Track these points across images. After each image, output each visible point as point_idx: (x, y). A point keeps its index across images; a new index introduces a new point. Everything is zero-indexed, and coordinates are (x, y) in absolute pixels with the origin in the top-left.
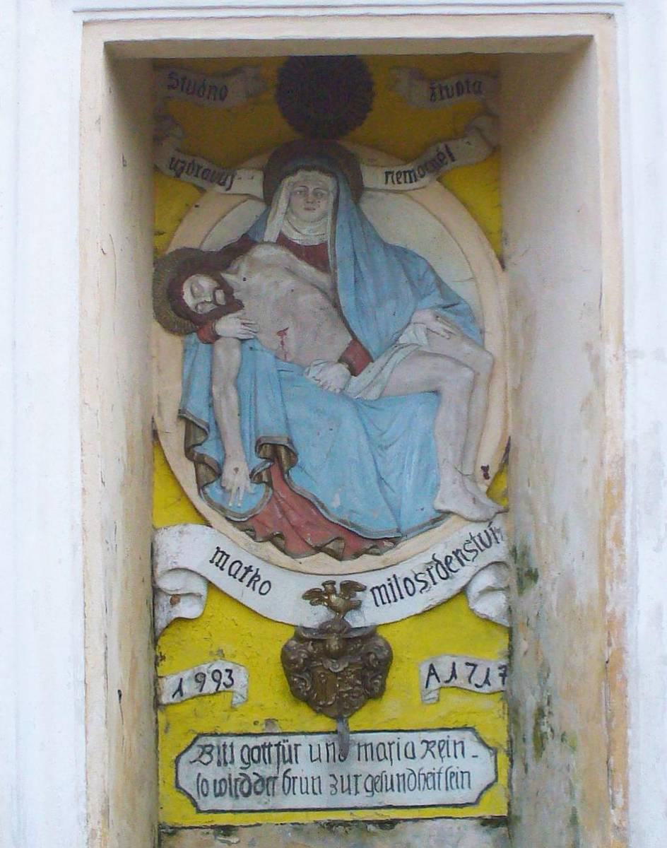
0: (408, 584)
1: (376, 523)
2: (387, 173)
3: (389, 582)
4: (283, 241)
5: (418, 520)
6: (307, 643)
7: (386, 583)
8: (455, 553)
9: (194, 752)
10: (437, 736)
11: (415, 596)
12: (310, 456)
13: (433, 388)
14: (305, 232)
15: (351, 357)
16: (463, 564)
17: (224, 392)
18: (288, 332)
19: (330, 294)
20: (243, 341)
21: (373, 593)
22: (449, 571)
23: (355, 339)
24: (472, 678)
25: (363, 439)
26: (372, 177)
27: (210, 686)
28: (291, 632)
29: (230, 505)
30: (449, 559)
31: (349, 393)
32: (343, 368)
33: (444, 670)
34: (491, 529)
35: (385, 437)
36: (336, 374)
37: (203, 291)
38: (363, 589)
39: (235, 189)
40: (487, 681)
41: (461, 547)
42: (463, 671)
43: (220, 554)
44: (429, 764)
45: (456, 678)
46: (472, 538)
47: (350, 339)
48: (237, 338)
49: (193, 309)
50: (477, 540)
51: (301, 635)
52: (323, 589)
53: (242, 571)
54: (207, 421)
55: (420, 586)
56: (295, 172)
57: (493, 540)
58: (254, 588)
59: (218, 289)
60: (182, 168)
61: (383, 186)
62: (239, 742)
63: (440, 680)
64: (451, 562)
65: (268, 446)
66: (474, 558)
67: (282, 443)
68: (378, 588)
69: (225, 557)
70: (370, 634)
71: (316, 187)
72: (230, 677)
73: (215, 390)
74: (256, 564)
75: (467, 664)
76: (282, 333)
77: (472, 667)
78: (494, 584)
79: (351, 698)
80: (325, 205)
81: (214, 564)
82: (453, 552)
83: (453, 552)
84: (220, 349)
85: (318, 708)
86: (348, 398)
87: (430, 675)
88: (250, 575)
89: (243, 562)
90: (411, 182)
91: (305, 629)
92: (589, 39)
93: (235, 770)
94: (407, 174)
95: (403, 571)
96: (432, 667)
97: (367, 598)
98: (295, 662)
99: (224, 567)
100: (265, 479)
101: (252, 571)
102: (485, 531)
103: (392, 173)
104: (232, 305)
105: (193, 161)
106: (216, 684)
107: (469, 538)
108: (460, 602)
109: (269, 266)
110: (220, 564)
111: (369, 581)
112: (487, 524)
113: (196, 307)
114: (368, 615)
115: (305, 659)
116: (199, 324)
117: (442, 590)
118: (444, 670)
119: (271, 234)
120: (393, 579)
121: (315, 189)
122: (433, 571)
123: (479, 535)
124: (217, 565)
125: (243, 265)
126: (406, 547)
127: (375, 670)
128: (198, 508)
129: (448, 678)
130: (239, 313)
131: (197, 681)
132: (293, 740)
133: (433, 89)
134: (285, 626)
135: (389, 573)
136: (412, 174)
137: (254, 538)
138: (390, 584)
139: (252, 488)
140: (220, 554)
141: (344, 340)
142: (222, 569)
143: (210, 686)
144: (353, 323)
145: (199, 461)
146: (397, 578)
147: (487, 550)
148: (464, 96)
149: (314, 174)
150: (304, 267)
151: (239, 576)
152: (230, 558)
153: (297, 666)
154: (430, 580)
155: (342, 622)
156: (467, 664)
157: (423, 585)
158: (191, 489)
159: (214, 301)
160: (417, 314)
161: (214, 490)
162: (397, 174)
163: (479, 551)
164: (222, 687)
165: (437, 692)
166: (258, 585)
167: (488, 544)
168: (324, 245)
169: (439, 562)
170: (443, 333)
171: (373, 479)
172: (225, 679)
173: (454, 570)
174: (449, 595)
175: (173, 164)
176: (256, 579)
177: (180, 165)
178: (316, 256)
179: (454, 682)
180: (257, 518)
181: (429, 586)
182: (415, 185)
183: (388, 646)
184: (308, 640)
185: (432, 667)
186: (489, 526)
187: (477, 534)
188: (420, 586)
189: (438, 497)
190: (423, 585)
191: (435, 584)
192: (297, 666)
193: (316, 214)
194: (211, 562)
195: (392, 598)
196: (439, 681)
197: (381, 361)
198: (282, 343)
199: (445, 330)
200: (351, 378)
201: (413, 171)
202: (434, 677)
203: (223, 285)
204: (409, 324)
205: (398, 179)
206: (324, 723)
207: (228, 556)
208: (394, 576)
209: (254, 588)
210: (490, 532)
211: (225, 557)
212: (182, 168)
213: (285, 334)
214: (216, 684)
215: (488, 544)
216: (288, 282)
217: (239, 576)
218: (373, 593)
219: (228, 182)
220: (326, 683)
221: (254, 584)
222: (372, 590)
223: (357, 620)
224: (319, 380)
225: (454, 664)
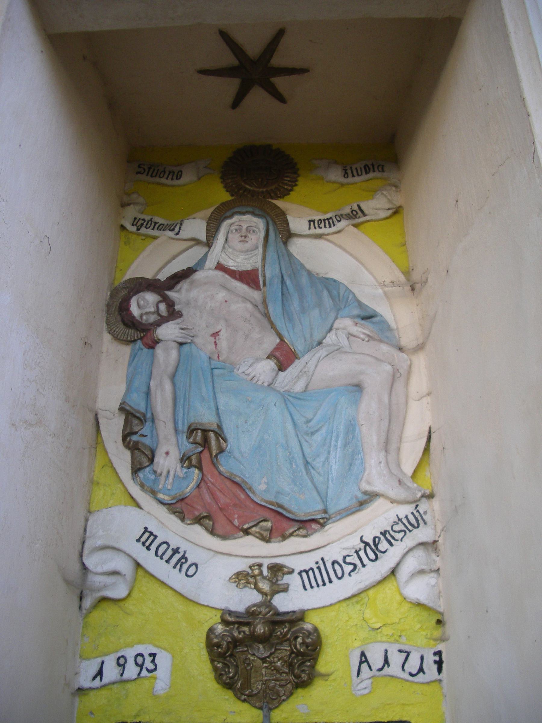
0: (337, 567)
2: (310, 221)
3: (317, 565)
4: (220, 267)
5: (344, 503)
6: (232, 627)
7: (315, 567)
8: (384, 533)
11: (343, 579)
13: (355, 381)
14: (239, 260)
15: (278, 354)
16: (391, 544)
17: (161, 384)
18: (221, 333)
19: (261, 307)
20: (181, 344)
21: (301, 577)
22: (377, 552)
23: (282, 340)
24: (405, 667)
25: (289, 426)
27: (131, 671)
29: (160, 487)
30: (377, 540)
31: (276, 387)
32: (271, 364)
33: (376, 661)
34: (418, 511)
35: (311, 424)
37: (148, 304)
38: (291, 572)
39: (182, 235)
40: (421, 670)
41: (389, 528)
42: (396, 659)
43: (147, 535)
45: (389, 666)
46: (400, 520)
47: (278, 341)
48: (175, 341)
49: (138, 318)
50: (405, 521)
52: (250, 572)
53: (170, 553)
54: (183, 469)
55: (348, 568)
56: (231, 217)
57: (421, 522)
58: (180, 570)
59: (160, 302)
60: (142, 224)
61: (308, 232)
63: (372, 668)
64: (379, 543)
65: (199, 431)
66: (403, 538)
67: (211, 429)
68: (307, 572)
69: (152, 537)
71: (248, 225)
72: (153, 661)
73: (152, 383)
74: (184, 546)
75: (400, 651)
76: (215, 335)
77: (406, 654)
78: (436, 544)
79: (277, 688)
81: (141, 542)
82: (381, 533)
83: (381, 533)
84: (159, 350)
85: (243, 697)
86: (275, 390)
87: (361, 662)
88: (177, 557)
89: (170, 544)
90: (330, 227)
91: (230, 613)
94: (327, 221)
96: (363, 654)
97: (294, 581)
98: (218, 645)
99: (151, 547)
100: (194, 462)
101: (179, 553)
102: (412, 513)
103: (314, 221)
105: (152, 219)
106: (139, 668)
107: (396, 520)
108: (389, 587)
109: (205, 284)
110: (147, 544)
112: (414, 505)
113: (141, 316)
115: (228, 643)
116: (143, 330)
118: (376, 661)
119: (211, 263)
120: (321, 562)
121: (247, 227)
122: (362, 553)
123: (406, 517)
124: (144, 544)
127: (303, 654)
128: (131, 493)
129: (380, 666)
130: (178, 321)
131: (119, 664)
133: (346, 170)
134: (211, 610)
135: (316, 556)
136: (331, 221)
137: (183, 520)
138: (319, 568)
139: (182, 472)
140: (147, 535)
141: (272, 341)
142: (148, 548)
143: (131, 671)
144: (280, 324)
146: (325, 561)
147: (415, 531)
148: (375, 173)
151: (166, 557)
152: (158, 539)
153: (219, 650)
154: (358, 563)
155: (268, 604)
156: (400, 651)
157: (351, 567)
158: (125, 472)
159: (157, 312)
160: (338, 321)
161: (146, 474)
162: (318, 221)
163: (407, 531)
164: (144, 673)
165: (370, 681)
166: (185, 567)
167: (416, 525)
169: (367, 544)
170: (362, 336)
171: (300, 462)
172: (148, 664)
173: (383, 550)
174: (379, 577)
175: (138, 223)
176: (183, 561)
177: (141, 222)
179: (386, 670)
180: (186, 501)
181: (358, 568)
182: (333, 229)
183: (316, 630)
184: (233, 623)
185: (363, 654)
186: (416, 508)
187: (405, 516)
188: (348, 568)
189: (364, 479)
190: (351, 567)
191: (364, 566)
192: (219, 650)
193: (248, 246)
194: (138, 540)
195: (320, 582)
196: (371, 670)
198: (216, 343)
199: (364, 334)
200: (277, 374)
201: (331, 218)
202: (365, 664)
203: (165, 299)
204: (330, 330)
205: (319, 226)
207: (156, 537)
208: (322, 559)
209: (180, 570)
210: (417, 514)
211: (152, 537)
212: (142, 224)
213: (218, 335)
214: (139, 668)
215: (416, 525)
216: (222, 295)
217: (166, 557)
218: (301, 577)
219: (177, 229)
220: (251, 669)
221: (181, 566)
222: (300, 573)
224: (249, 375)
225: (386, 652)
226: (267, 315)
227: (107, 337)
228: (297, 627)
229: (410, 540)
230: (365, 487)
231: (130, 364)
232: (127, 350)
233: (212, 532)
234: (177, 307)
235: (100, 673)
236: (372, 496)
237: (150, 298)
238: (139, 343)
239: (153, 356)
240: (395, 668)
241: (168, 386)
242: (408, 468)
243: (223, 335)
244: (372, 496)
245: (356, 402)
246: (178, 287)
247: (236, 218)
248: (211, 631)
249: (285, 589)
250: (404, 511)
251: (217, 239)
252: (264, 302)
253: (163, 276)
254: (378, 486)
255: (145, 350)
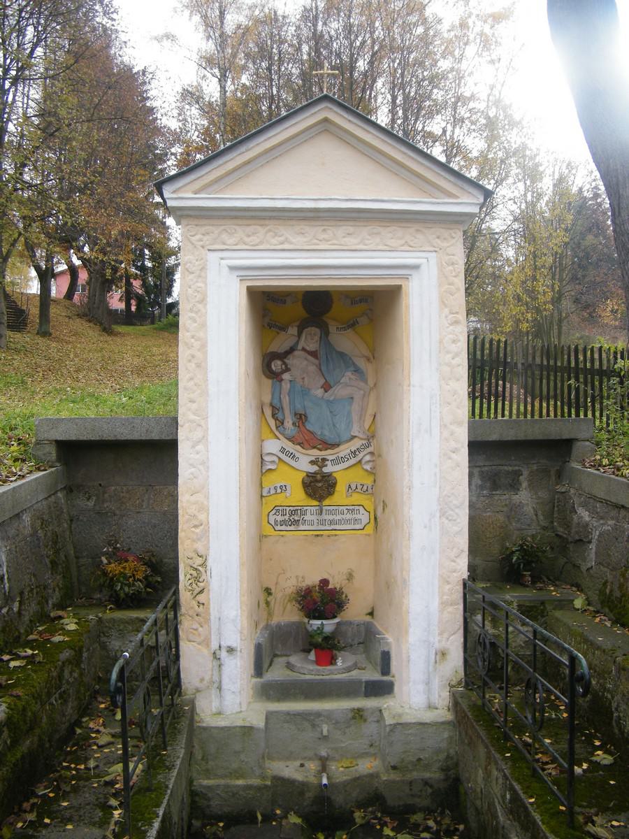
1: (328, 435)
4: (304, 349)
5: (345, 439)
9: (274, 511)
10: (351, 508)
12: (312, 417)
23: (326, 381)
26: (332, 329)
28: (305, 474)
32: (322, 390)
33: (354, 487)
36: (320, 392)
38: (328, 460)
42: (359, 487)
44: (349, 516)
51: (309, 475)
62: (288, 509)
70: (330, 475)
73: (281, 396)
74: (294, 452)
76: (303, 379)
80: (317, 338)
84: (283, 384)
92: (401, 286)
93: (287, 517)
95: (341, 455)
97: (329, 463)
104: (287, 370)
111: (330, 458)
114: (328, 469)
117: (353, 461)
118: (354, 487)
119: (300, 347)
125: (290, 356)
126: (342, 447)
132: (305, 508)
135: (336, 456)
139: (293, 428)
141: (323, 381)
143: (279, 490)
144: (326, 375)
145: (276, 419)
149: (313, 328)
150: (310, 358)
168: (317, 351)
171: (332, 425)
178: (314, 354)
197: (334, 388)
206: (316, 503)
216: (305, 362)
223: (325, 470)
226: (320, 370)
227: (263, 376)
228: (525, 484)
229: (365, 452)
230: (352, 434)
231: (272, 387)
232: (270, 381)
233: (303, 448)
234: (289, 366)
235: (269, 492)
236: (354, 437)
237: (279, 363)
238: (275, 380)
239: (281, 385)
240: (359, 490)
241: (287, 397)
242: (367, 428)
243: (306, 379)
244: (354, 437)
245: (351, 404)
246: (289, 356)
247: (309, 329)
248: (303, 479)
249: (326, 466)
250: (364, 442)
251: (392, 441)
252: (320, 364)
253: (281, 350)
254: (356, 434)
255: (278, 383)
